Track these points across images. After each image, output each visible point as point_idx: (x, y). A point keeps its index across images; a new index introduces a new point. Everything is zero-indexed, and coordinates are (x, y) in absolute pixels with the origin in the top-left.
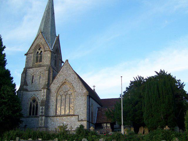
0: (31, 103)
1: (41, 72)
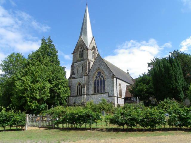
0: (78, 87)
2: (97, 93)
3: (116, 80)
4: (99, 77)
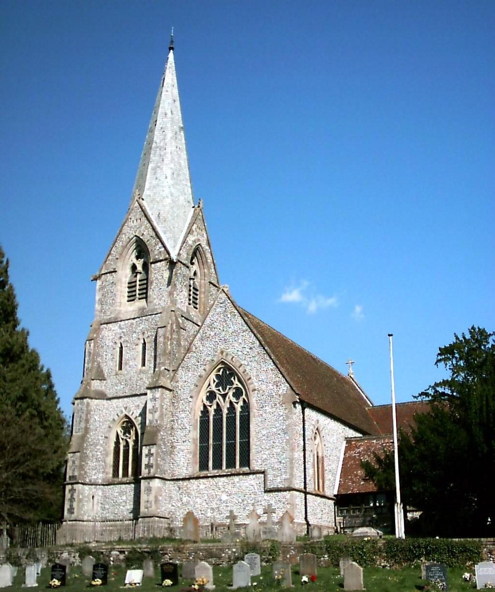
0: (118, 436)
1: (143, 333)
2: (212, 472)
3: (303, 409)
4: (224, 396)
